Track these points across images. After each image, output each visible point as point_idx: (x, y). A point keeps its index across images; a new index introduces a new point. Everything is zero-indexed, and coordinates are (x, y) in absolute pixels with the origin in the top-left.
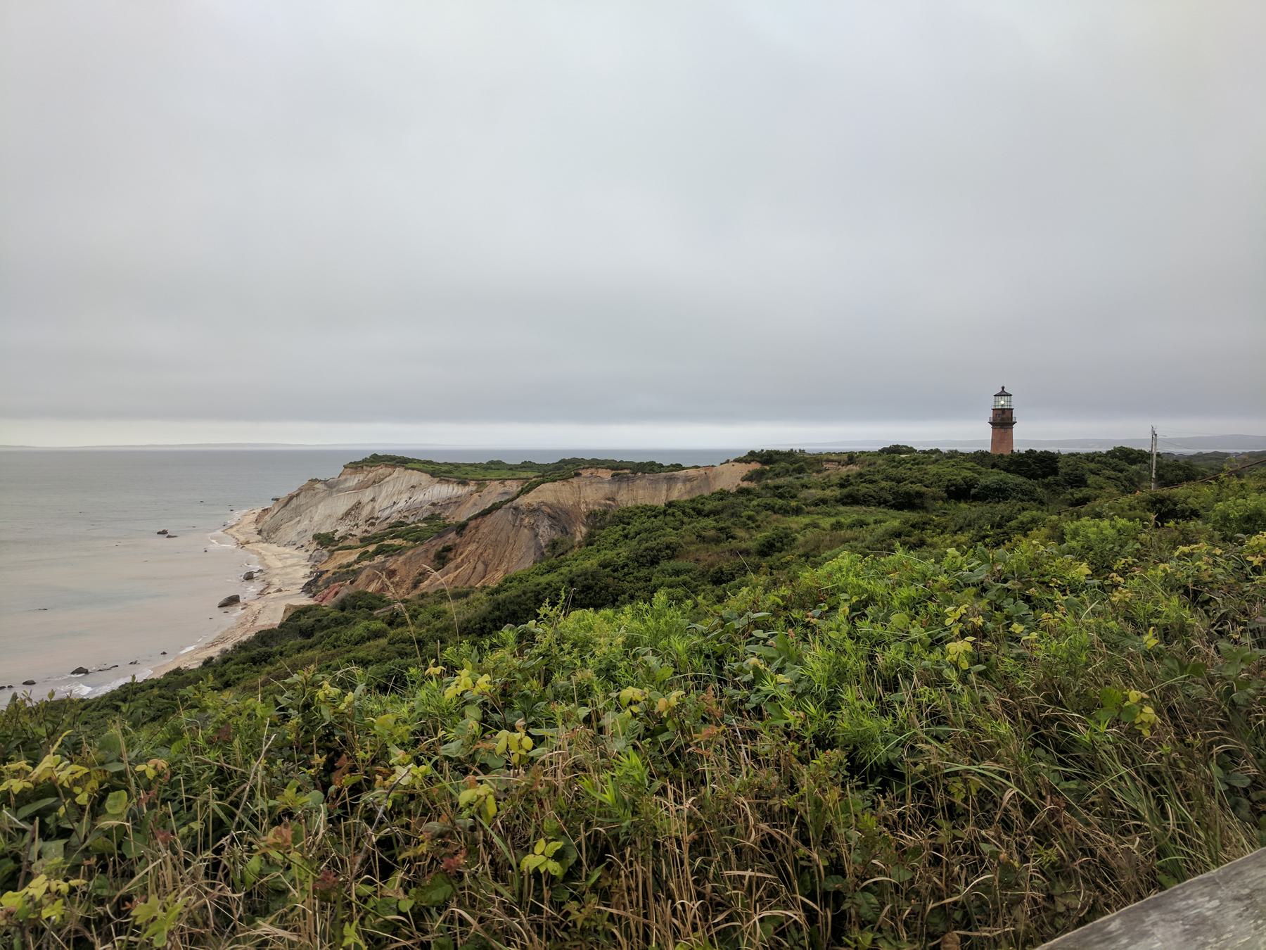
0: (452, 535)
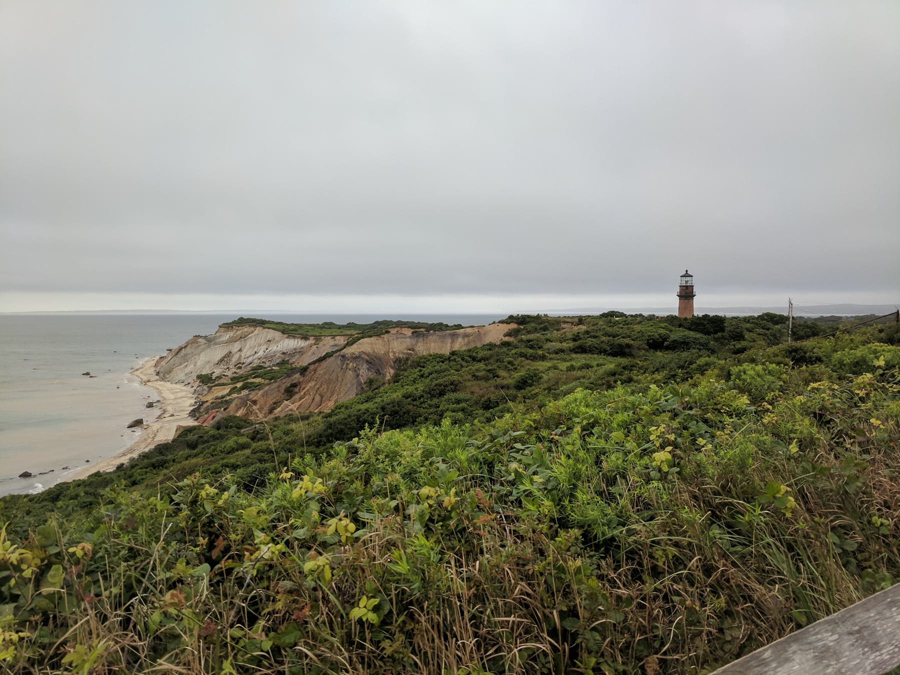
0: (297, 375)
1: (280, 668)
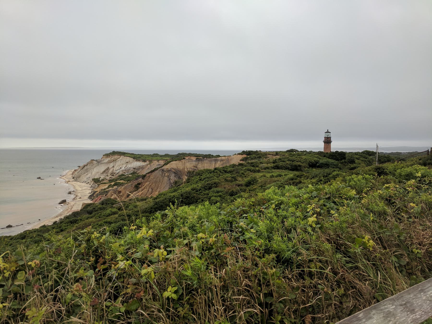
0: (141, 179)
1: (129, 321)
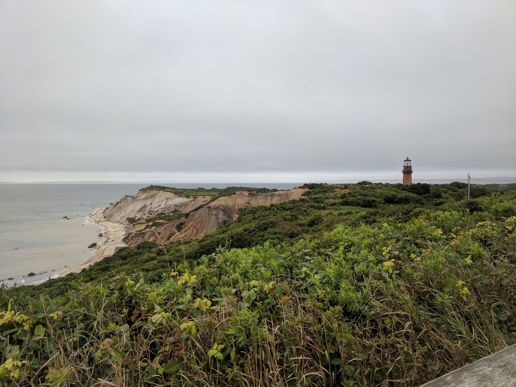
0: (183, 218)
1: (168, 384)
